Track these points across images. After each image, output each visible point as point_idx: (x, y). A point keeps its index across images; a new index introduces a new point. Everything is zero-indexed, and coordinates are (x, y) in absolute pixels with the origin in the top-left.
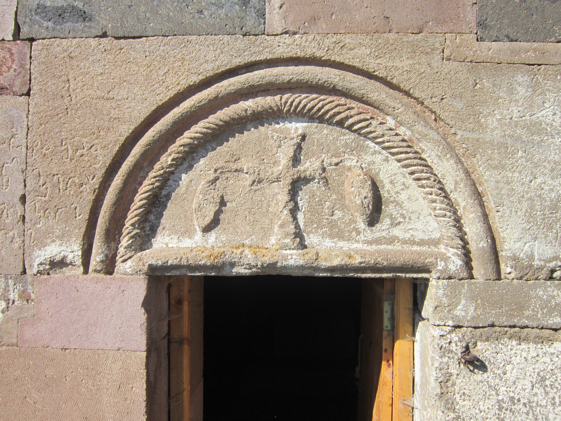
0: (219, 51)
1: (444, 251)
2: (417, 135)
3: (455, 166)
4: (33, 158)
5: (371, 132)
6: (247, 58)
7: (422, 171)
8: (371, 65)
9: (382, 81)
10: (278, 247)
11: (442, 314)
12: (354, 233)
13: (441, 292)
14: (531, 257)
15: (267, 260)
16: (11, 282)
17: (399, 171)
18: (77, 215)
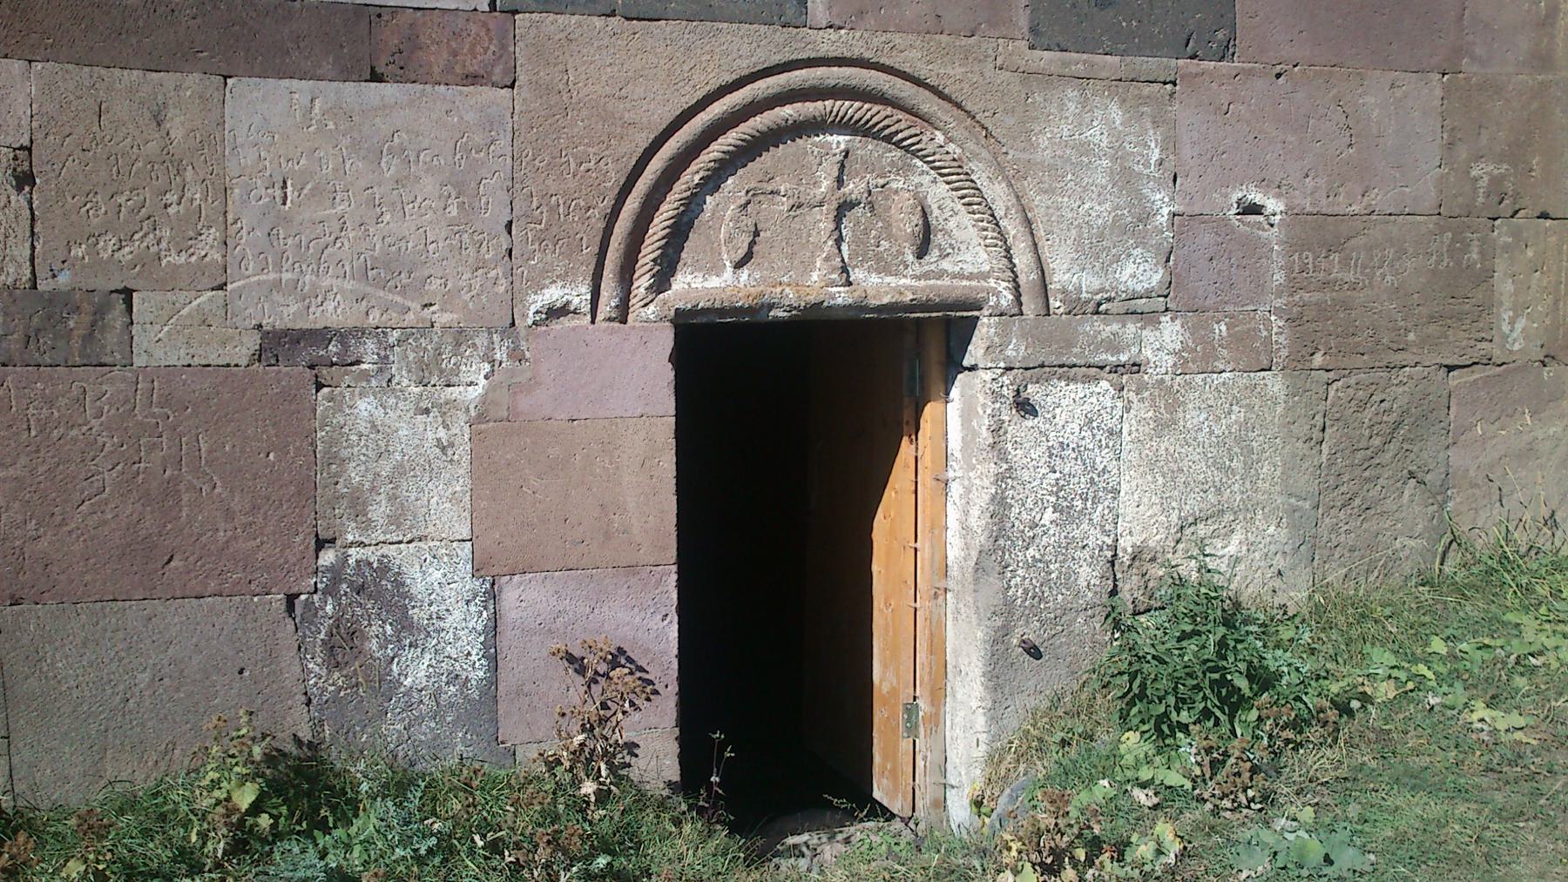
0: (755, 44)
1: (995, 286)
2: (968, 154)
3: (1006, 189)
4: (522, 172)
5: (922, 150)
6: (787, 55)
7: (974, 196)
8: (922, 71)
9: (934, 90)
10: (823, 284)
11: (994, 355)
12: (901, 267)
13: (993, 330)
14: (1079, 290)
15: (812, 299)
16: (496, 338)
17: (947, 195)
18: (584, 247)
